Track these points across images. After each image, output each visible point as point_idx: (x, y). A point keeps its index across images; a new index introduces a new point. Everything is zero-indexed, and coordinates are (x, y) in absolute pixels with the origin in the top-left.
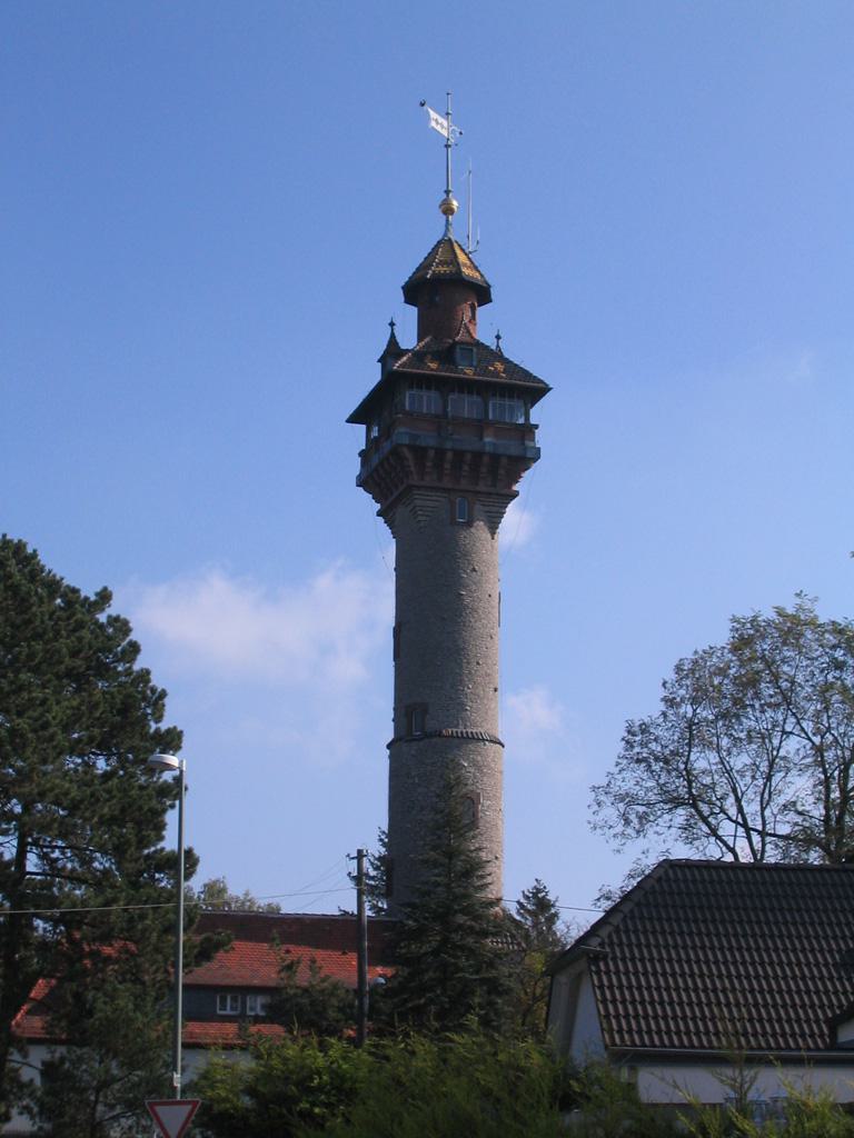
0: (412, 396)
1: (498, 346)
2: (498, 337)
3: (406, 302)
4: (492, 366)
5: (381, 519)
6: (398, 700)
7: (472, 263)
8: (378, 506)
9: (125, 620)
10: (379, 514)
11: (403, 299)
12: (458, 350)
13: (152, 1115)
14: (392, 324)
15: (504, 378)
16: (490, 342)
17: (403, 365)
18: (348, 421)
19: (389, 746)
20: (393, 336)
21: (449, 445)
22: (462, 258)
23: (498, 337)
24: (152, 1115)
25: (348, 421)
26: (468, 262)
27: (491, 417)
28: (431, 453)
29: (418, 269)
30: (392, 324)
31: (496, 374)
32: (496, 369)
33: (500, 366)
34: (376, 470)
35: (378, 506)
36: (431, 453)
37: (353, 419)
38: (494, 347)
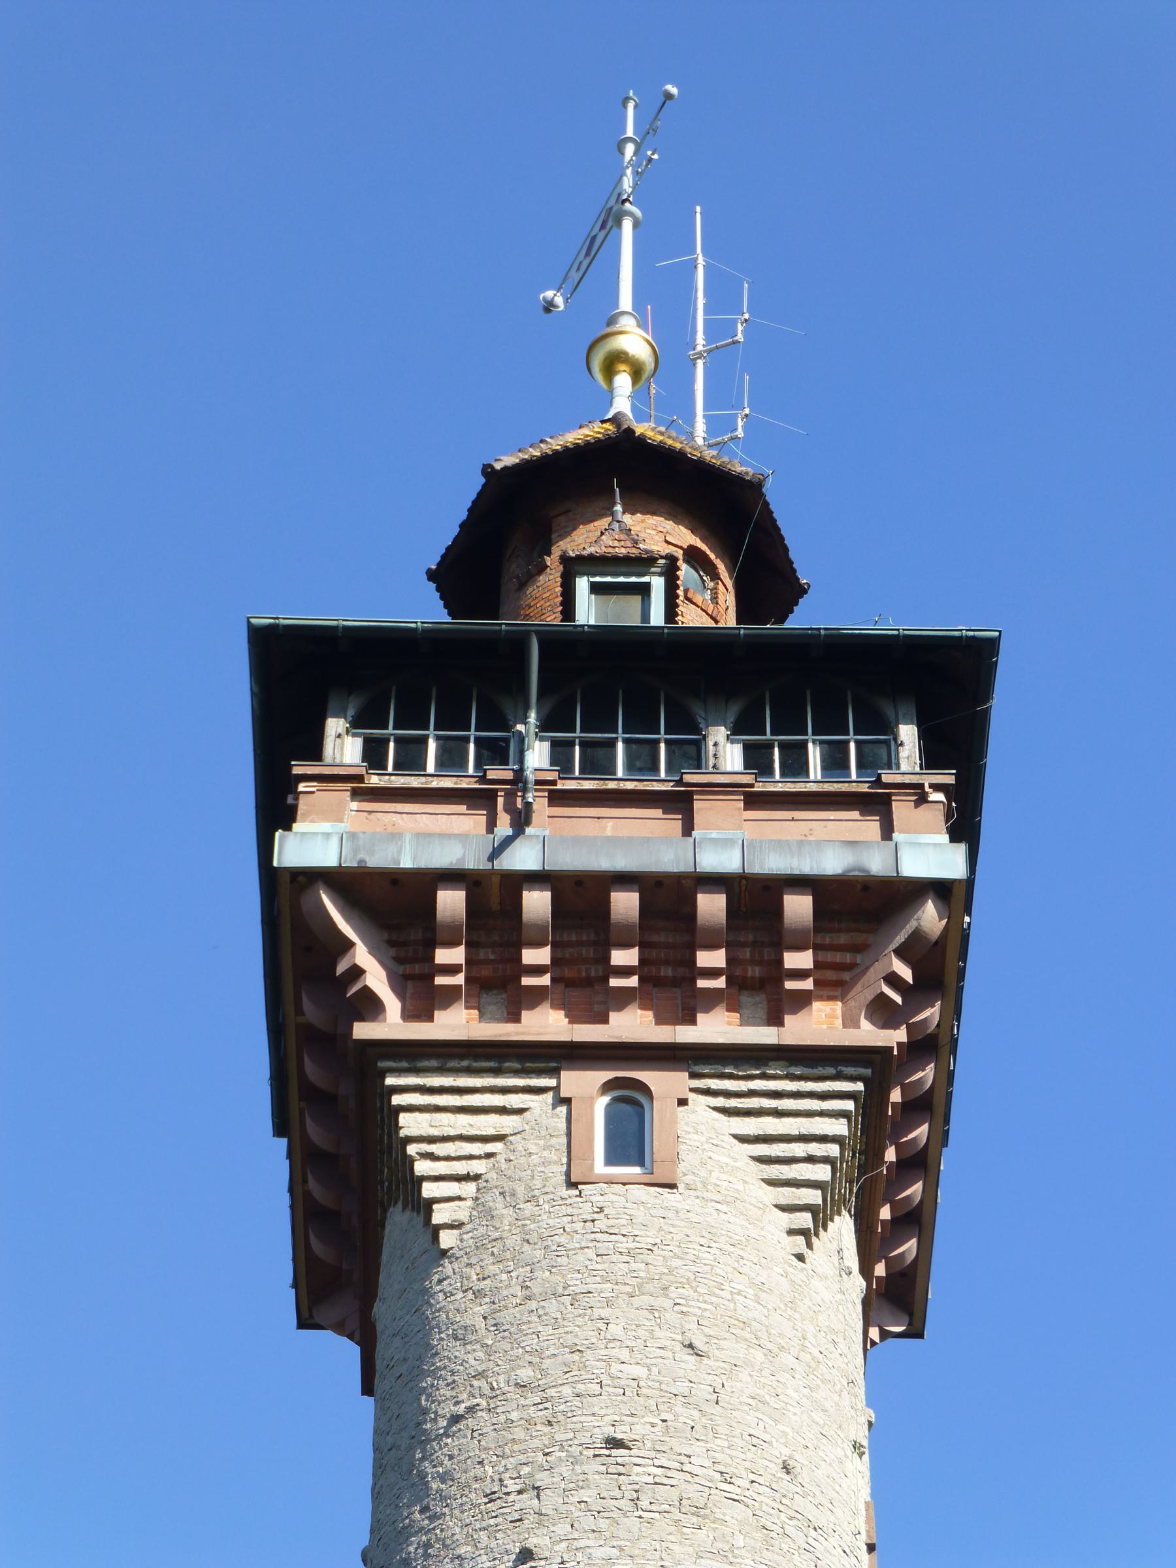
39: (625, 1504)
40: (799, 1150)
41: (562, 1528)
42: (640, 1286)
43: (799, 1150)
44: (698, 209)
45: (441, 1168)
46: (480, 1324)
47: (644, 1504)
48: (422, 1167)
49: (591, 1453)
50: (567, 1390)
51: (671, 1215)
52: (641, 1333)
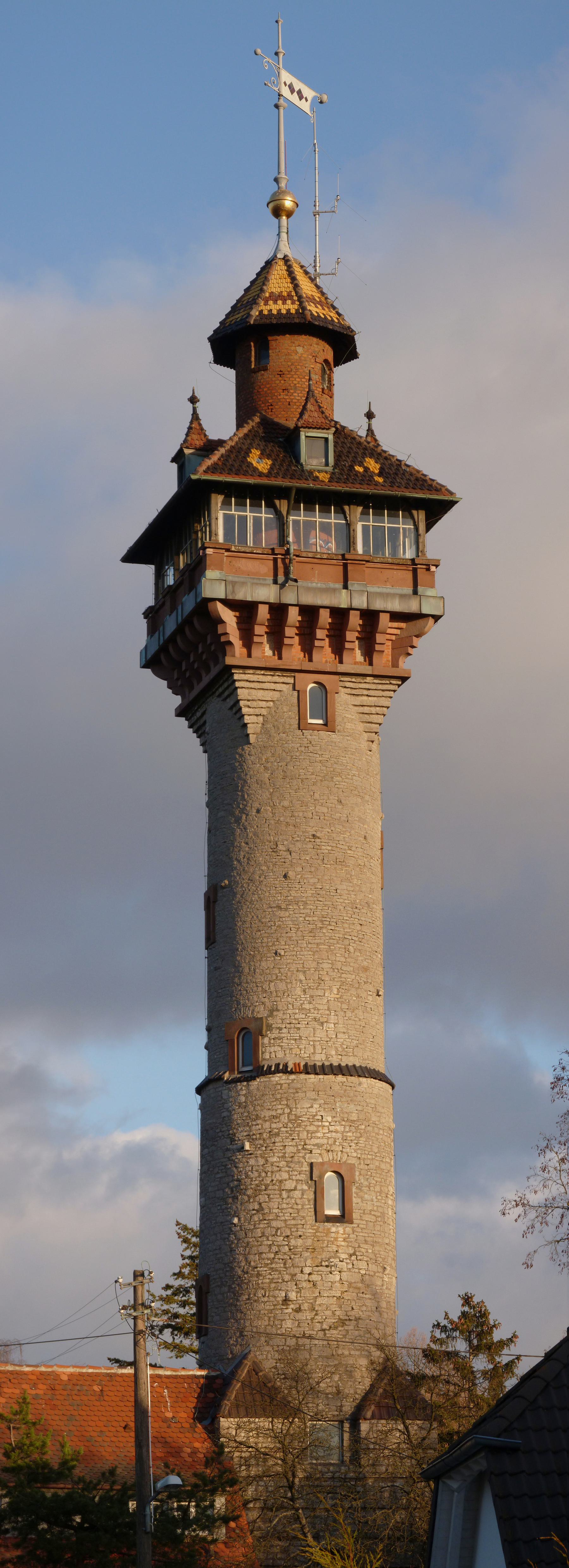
0: (228, 519)
1: (370, 431)
2: (370, 415)
3: (210, 339)
4: (361, 464)
5: (183, 722)
6: (202, 1127)
7: (323, 294)
8: (177, 700)
9: (145, 618)
10: (181, 712)
11: (210, 355)
12: (303, 437)
13: (202, 721)
14: (193, 400)
15: (380, 486)
16: (357, 425)
17: (213, 469)
18: (127, 559)
19: (199, 1090)
20: (195, 417)
21: (289, 597)
22: (307, 287)
23: (370, 415)
24: (202, 721)
25: (127, 559)
26: (317, 295)
27: (360, 549)
28: (263, 613)
29: (234, 308)
30: (193, 400)
31: (367, 477)
32: (366, 469)
33: (373, 465)
34: (172, 639)
35: (177, 700)
36: (263, 613)
37: (134, 555)
38: (363, 433)
39: (320, 862)
40: (373, 710)
41: (299, 869)
42: (324, 777)
43: (373, 710)
44: (252, 344)
45: (251, 711)
46: (267, 781)
47: (325, 861)
48: (245, 710)
49: (308, 840)
50: (301, 814)
51: (333, 744)
52: (325, 797)
